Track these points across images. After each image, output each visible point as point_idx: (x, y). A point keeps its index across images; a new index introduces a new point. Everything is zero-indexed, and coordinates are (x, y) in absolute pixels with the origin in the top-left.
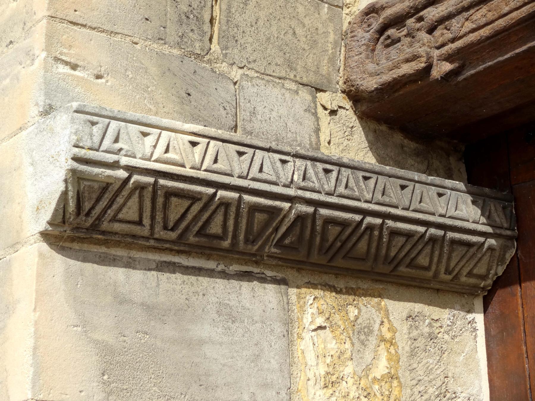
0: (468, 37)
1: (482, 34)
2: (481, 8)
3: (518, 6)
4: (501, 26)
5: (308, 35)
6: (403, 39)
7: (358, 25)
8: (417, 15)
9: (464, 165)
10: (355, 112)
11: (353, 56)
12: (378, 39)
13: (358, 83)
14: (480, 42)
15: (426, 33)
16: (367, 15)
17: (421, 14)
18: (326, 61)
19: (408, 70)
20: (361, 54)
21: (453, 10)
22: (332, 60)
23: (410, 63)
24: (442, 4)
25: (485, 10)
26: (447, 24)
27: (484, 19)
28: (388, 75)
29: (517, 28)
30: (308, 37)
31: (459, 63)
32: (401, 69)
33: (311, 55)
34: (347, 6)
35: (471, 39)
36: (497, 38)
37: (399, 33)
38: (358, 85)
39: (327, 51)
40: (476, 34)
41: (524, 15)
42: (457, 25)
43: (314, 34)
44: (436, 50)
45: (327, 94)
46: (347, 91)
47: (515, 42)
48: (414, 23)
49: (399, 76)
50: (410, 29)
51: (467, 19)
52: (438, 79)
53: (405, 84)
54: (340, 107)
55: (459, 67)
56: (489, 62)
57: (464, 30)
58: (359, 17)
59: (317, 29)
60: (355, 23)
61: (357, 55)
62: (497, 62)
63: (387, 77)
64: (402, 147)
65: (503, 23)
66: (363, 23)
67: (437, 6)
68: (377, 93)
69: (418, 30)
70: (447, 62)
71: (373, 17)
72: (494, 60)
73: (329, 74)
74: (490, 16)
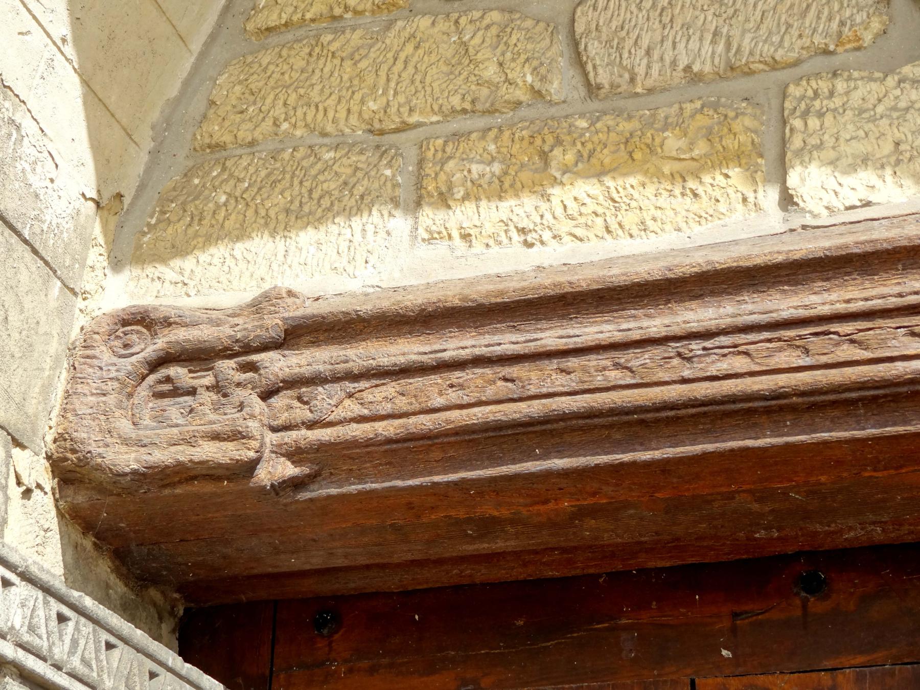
0: (347, 427)
1: (380, 431)
2: (383, 384)
3: (464, 403)
4: (423, 427)
5: (24, 329)
6: (204, 393)
7: (103, 337)
8: (244, 358)
9: (177, 642)
10: (56, 500)
11: (85, 394)
12: (143, 378)
13: (90, 448)
14: (369, 443)
15: (258, 396)
16: (124, 325)
17: (255, 357)
18: (37, 390)
19: (216, 456)
20: (104, 395)
21: (325, 371)
22: (46, 389)
23: (222, 443)
24: (297, 352)
25: (393, 390)
26: (304, 392)
27: (389, 405)
28: (166, 453)
29: (452, 439)
30: (24, 333)
31: (311, 469)
32: (198, 449)
33: (20, 371)
34: (84, 295)
35: (354, 434)
36: (406, 445)
37: (192, 378)
38: (89, 452)
39: (43, 370)
40: (367, 426)
41: (475, 422)
42: (327, 400)
43: (32, 332)
44: (270, 432)
45: (27, 452)
46: (54, 457)
47: (435, 461)
48: (233, 369)
49: (191, 461)
50: (224, 378)
51: (350, 395)
52: (265, 487)
53: (194, 478)
54: (39, 486)
55: (308, 476)
56: (372, 483)
57: (339, 413)
58: (108, 324)
59: (38, 323)
60: (98, 333)
61: (92, 394)
62: (390, 487)
63: (163, 456)
64: (108, 586)
65: (428, 424)
66: (113, 337)
67: (286, 352)
68: (132, 480)
69: (238, 385)
70: (289, 460)
71: (138, 332)
72: (383, 482)
73: (36, 416)
74: (402, 404)
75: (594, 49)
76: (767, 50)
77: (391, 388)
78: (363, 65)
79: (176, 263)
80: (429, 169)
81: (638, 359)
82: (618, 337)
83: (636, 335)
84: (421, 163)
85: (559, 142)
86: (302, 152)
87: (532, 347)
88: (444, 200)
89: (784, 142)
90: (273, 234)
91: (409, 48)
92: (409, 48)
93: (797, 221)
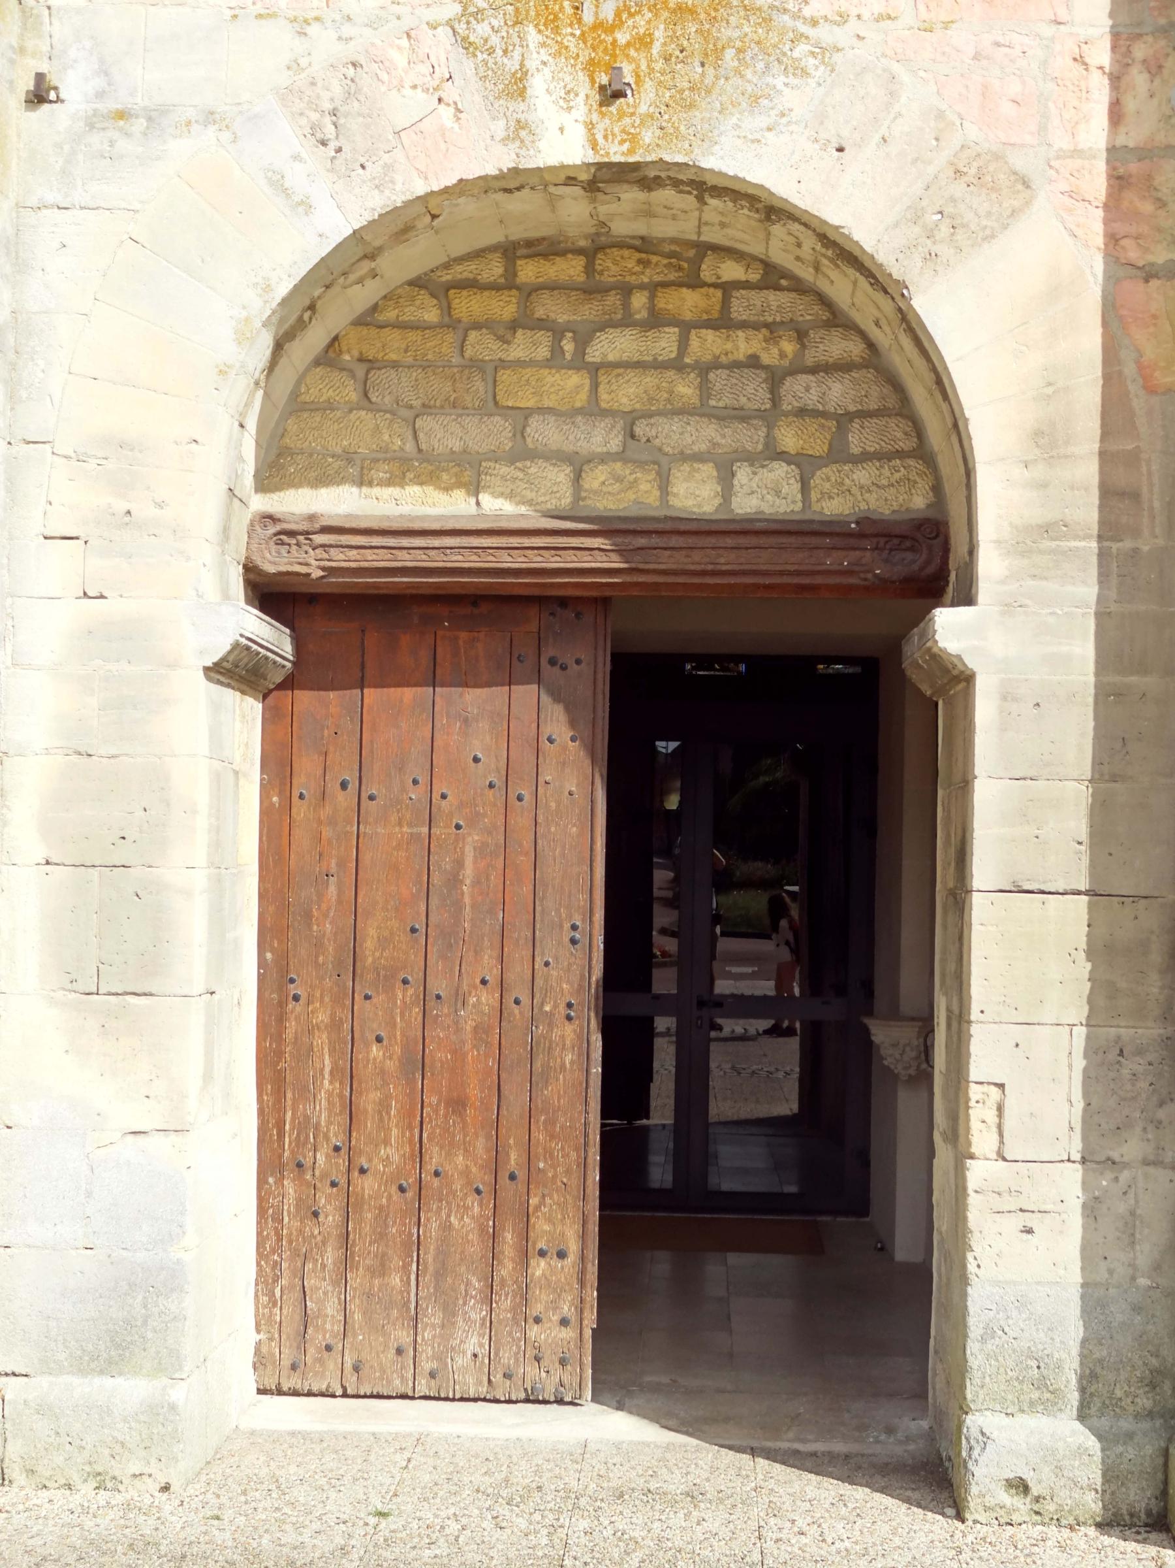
14: (347, 569)
17: (310, 536)
63: (283, 569)
74: (358, 557)
75: (421, 435)
76: (477, 448)
77: (355, 552)
78: (342, 425)
79: (278, 493)
80: (365, 471)
81: (432, 553)
82: (426, 545)
83: (431, 546)
84: (362, 468)
85: (408, 470)
86: (320, 457)
87: (399, 545)
88: (370, 484)
89: (479, 482)
90: (312, 487)
91: (358, 423)
92: (358, 423)
93: (480, 512)
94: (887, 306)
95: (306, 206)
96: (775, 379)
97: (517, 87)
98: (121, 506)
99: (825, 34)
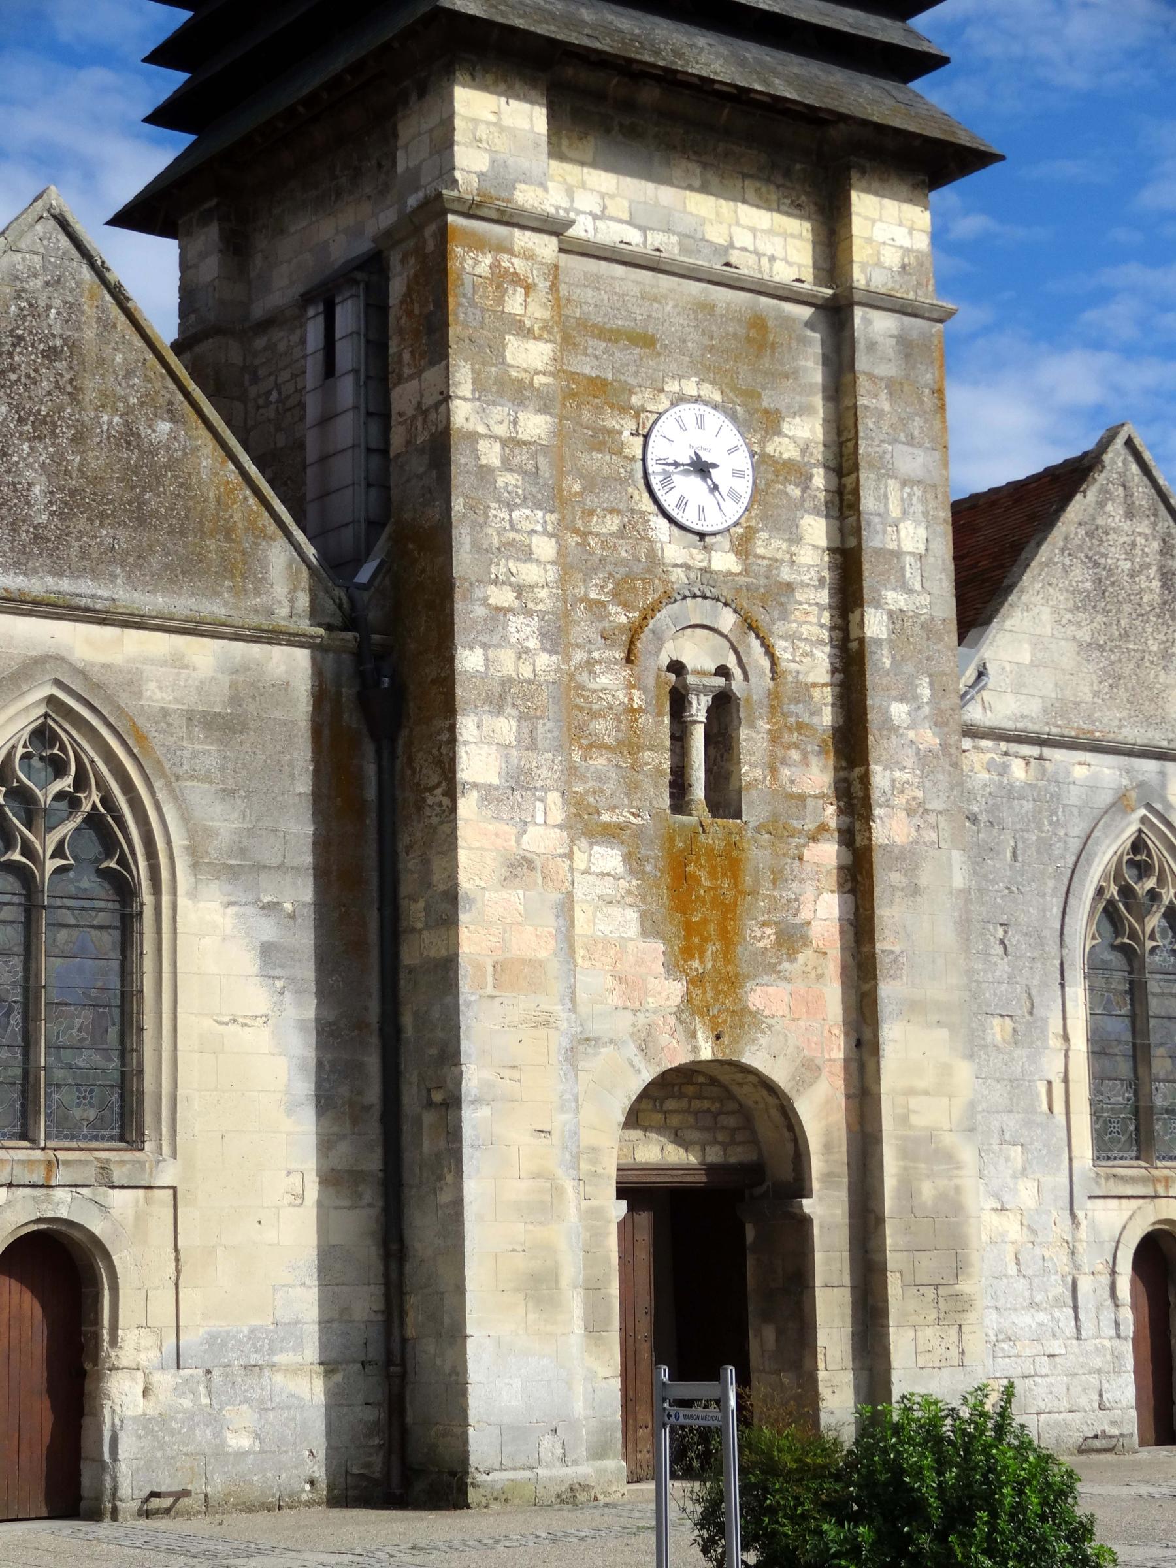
94: (771, 1100)
95: (639, 1071)
96: (715, 1116)
97: (693, 1035)
98: (593, 1169)
99: (769, 1021)
